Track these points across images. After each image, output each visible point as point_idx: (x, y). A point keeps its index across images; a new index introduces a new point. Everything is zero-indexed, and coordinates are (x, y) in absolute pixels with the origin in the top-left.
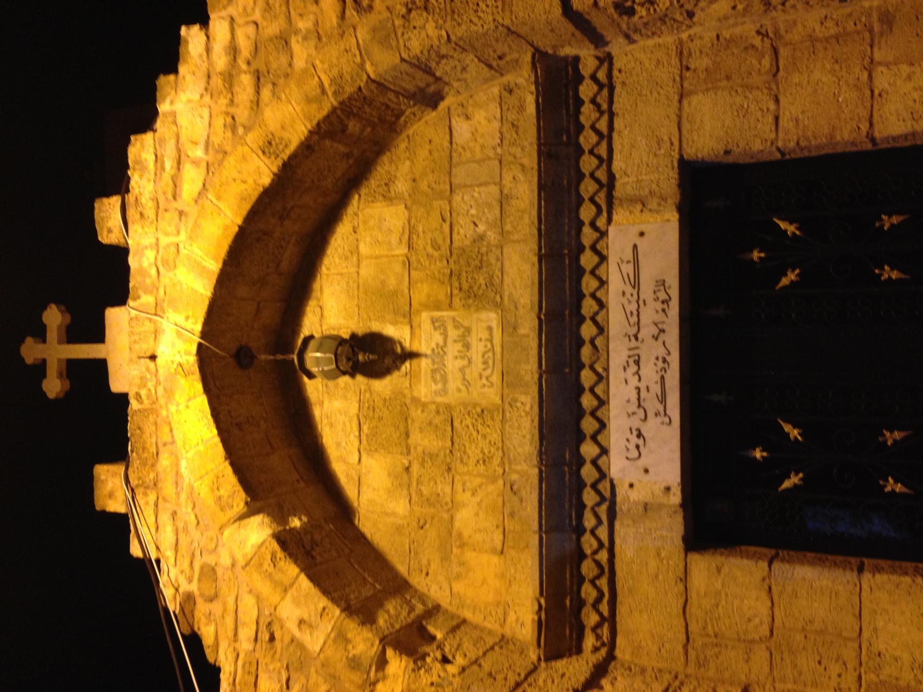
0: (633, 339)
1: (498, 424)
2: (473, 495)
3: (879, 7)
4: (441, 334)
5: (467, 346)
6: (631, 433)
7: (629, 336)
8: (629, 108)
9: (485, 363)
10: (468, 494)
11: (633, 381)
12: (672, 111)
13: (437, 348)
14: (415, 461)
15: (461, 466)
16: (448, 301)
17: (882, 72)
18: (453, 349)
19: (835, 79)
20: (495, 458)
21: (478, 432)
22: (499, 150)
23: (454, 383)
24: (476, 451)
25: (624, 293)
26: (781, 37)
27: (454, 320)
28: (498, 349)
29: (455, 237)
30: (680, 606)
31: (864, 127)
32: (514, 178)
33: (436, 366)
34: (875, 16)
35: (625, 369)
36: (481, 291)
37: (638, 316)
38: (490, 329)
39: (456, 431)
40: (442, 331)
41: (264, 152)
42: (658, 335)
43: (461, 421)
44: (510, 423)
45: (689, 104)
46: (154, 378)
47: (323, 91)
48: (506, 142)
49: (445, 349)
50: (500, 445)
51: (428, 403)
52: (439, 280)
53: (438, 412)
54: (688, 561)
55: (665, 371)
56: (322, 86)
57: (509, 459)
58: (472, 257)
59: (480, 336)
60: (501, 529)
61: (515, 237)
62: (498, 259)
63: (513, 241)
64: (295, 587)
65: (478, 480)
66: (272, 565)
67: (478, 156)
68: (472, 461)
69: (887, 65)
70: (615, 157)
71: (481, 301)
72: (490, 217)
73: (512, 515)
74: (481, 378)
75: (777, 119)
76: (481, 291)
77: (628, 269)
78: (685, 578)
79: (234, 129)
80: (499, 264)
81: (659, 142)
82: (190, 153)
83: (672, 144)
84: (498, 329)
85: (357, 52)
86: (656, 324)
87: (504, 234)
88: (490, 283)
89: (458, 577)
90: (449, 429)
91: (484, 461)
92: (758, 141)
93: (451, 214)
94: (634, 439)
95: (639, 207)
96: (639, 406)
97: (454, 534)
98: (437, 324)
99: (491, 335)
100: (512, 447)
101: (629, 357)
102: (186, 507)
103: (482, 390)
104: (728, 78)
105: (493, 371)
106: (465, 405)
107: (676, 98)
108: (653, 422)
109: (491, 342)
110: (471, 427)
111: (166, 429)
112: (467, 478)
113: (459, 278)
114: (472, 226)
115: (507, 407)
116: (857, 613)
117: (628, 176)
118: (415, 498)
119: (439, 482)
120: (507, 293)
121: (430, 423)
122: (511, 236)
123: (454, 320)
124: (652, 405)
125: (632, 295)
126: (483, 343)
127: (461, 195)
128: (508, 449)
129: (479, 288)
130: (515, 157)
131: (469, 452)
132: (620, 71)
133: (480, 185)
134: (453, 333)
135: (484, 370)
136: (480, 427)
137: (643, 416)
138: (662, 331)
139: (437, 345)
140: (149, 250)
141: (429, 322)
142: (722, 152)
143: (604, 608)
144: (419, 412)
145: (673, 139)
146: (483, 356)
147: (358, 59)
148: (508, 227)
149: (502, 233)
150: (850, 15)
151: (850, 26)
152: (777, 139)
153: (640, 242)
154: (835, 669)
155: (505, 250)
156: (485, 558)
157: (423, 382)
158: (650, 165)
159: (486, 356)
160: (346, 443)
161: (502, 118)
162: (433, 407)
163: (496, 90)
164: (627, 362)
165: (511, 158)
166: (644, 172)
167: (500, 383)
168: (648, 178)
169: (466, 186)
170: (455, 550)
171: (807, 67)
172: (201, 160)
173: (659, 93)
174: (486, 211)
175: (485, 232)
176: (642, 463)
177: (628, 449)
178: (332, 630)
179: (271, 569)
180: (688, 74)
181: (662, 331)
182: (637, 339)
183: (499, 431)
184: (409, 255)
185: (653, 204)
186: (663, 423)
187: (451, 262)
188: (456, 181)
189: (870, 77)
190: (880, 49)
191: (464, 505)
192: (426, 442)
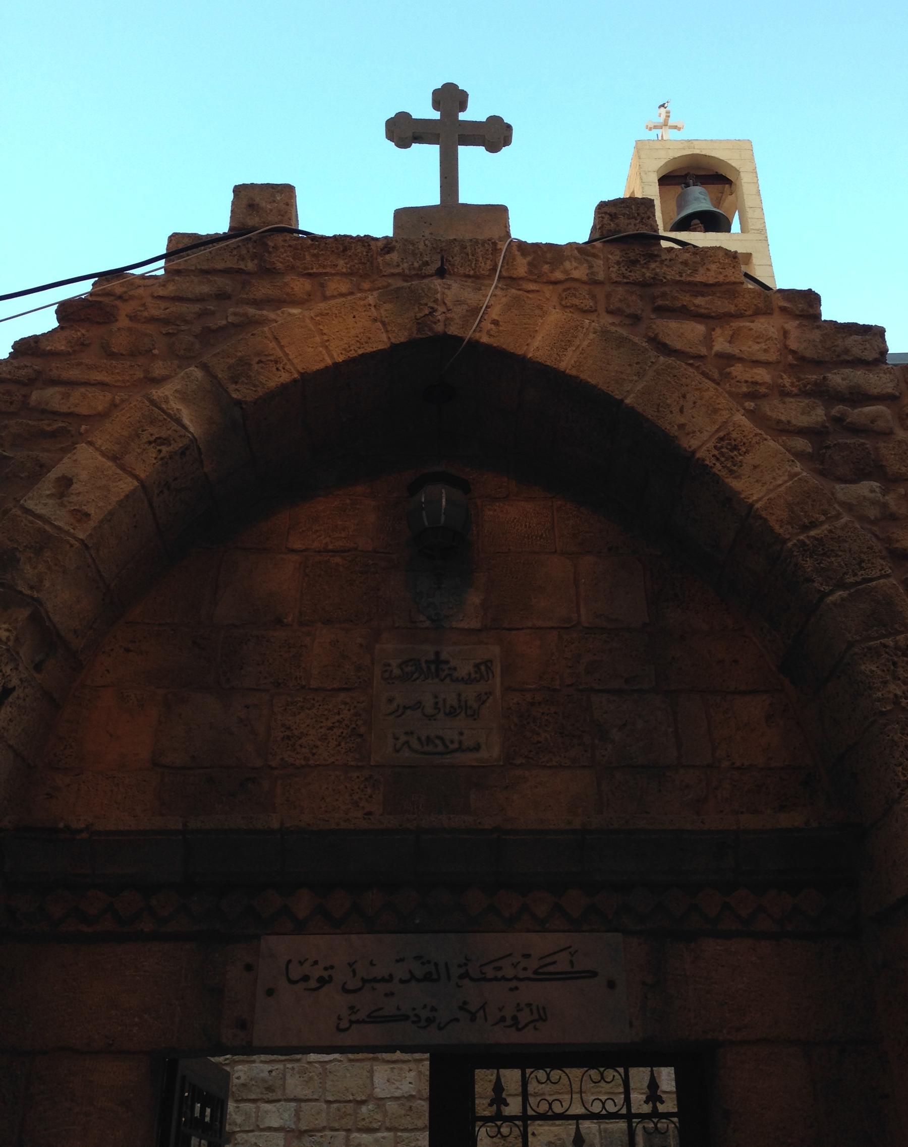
0: (462, 970)
4: (470, 674)
5: (452, 713)
6: (326, 969)
7: (466, 965)
9: (429, 740)
13: (450, 669)
21: (331, 729)
25: (527, 956)
27: (489, 694)
33: (424, 665)
35: (418, 958)
37: (496, 979)
40: (473, 676)
41: (721, 439)
42: (469, 1012)
43: (346, 704)
46: (413, 272)
47: (805, 528)
49: (448, 681)
50: (311, 762)
55: (413, 1022)
56: (814, 525)
64: (119, 471)
66: (152, 439)
74: (406, 733)
79: (752, 396)
82: (718, 331)
85: (859, 579)
86: (483, 1007)
91: (288, 738)
94: (318, 972)
96: (364, 981)
98: (483, 668)
99: (470, 750)
101: (436, 965)
102: (235, 314)
109: (460, 749)
110: (337, 717)
111: (344, 288)
123: (489, 694)
135: (419, 739)
137: (350, 986)
139: (455, 669)
140: (587, 271)
147: (850, 579)
159: (438, 742)
160: (317, 531)
164: (429, 962)
172: (710, 348)
177: (301, 963)
178: (58, 528)
179: (145, 437)
181: (473, 1019)
183: (332, 760)
186: (339, 1018)
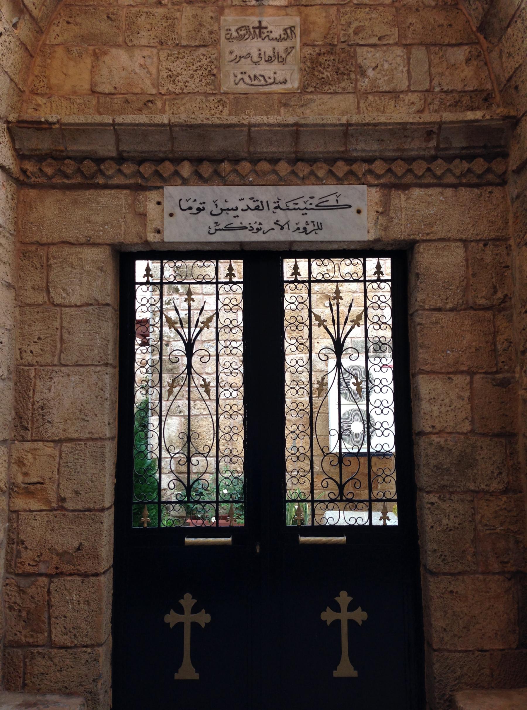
0: (276, 205)
1: (203, 89)
2: (141, 65)
3: (513, 377)
5: (269, 60)
6: (201, 204)
8: (461, 200)
10: (142, 61)
11: (242, 205)
12: (454, 234)
14: (167, 10)
15: (166, 55)
16: (309, 42)
17: (465, 379)
18: (267, 47)
19: (464, 348)
20: (174, 86)
21: (196, 71)
22: (437, 89)
23: (238, 48)
24: (179, 69)
26: (500, 311)
28: (267, 89)
29: (365, 49)
30: (68, 239)
31: (427, 368)
32: (413, 103)
34: (508, 375)
36: (316, 73)
37: (295, 209)
38: (285, 82)
39: (195, 50)
40: (283, 36)
43: (204, 55)
44: (204, 101)
45: (458, 247)
48: (444, 96)
51: (219, 23)
52: (327, 34)
53: (211, 33)
54: (105, 246)
57: (174, 99)
58: (347, 65)
59: (278, 72)
60: (113, 91)
61: (362, 105)
62: (344, 89)
63: (358, 103)
65: (154, 71)
67: (434, 71)
68: (170, 65)
69: (471, 382)
70: (423, 189)
71: (308, 74)
72: (380, 82)
73: (127, 101)
75: (439, 310)
76: (316, 73)
77: (332, 201)
78: (90, 243)
80: (340, 90)
81: (431, 225)
83: (428, 234)
84: (284, 89)
86: (287, 223)
87: (365, 95)
88: (325, 82)
89: (68, 51)
90: (197, 43)
91: (171, 77)
92: (423, 297)
93: (385, 45)
95: (380, 210)
96: (222, 210)
97: (106, 48)
98: (289, 31)
100: (184, 101)
101: (261, 202)
103: (232, 75)
104: (474, 275)
105: (248, 84)
106: (218, 59)
107: (464, 237)
108: (210, 221)
110: (199, 64)
112: (155, 60)
113: (328, 52)
114: (374, 65)
115: (219, 97)
116: (80, 363)
117: (405, 201)
118: (134, 10)
119: (149, 33)
120: (315, 97)
121: (201, 25)
122: (363, 101)
124: (224, 220)
125: (311, 204)
126: (272, 75)
127: (402, 54)
128: (182, 99)
129: (320, 71)
130: (430, 104)
131: (178, 62)
132: (491, 192)
133: (409, 72)
134: (281, 47)
136: (200, 72)
138: (282, 228)
141: (292, 24)
142: (417, 271)
143: (58, 180)
144: (211, 14)
145: (431, 235)
146: (261, 75)
148: (371, 98)
149: (366, 93)
150: (510, 359)
151: (502, 359)
152: (425, 309)
153: (353, 210)
154: (36, 349)
155: (351, 96)
156: (86, 76)
157: (237, 18)
158: (413, 217)
159: (261, 78)
161: (465, 92)
162: (216, 28)
163: (489, 86)
165: (429, 100)
166: (408, 213)
167: (239, 91)
168: (403, 216)
169: (409, 59)
170: (91, 48)
171: (475, 330)
173: (469, 223)
174: (386, 78)
175: (368, 77)
176: (178, 211)
180: (481, 245)
181: (282, 228)
182: (275, 208)
183: (197, 90)
184: (351, 4)
185: (382, 220)
187: (344, 46)
188: (414, 50)
189: (462, 372)
190: (483, 378)
191: (131, 57)
192: (184, 21)
